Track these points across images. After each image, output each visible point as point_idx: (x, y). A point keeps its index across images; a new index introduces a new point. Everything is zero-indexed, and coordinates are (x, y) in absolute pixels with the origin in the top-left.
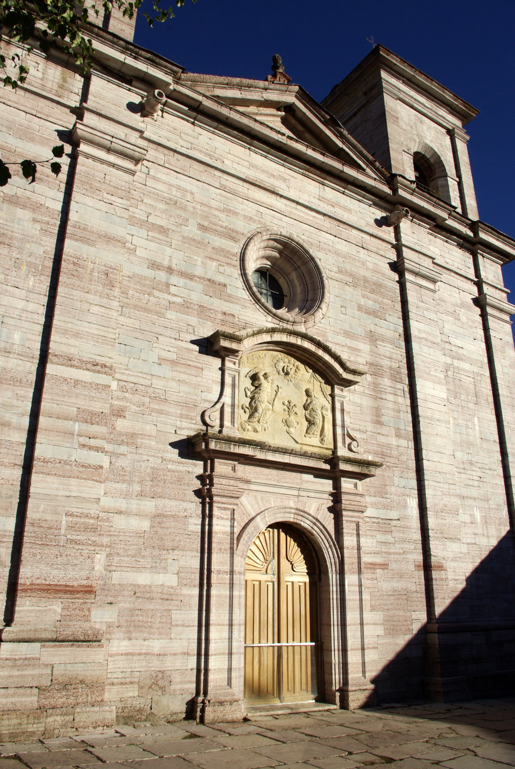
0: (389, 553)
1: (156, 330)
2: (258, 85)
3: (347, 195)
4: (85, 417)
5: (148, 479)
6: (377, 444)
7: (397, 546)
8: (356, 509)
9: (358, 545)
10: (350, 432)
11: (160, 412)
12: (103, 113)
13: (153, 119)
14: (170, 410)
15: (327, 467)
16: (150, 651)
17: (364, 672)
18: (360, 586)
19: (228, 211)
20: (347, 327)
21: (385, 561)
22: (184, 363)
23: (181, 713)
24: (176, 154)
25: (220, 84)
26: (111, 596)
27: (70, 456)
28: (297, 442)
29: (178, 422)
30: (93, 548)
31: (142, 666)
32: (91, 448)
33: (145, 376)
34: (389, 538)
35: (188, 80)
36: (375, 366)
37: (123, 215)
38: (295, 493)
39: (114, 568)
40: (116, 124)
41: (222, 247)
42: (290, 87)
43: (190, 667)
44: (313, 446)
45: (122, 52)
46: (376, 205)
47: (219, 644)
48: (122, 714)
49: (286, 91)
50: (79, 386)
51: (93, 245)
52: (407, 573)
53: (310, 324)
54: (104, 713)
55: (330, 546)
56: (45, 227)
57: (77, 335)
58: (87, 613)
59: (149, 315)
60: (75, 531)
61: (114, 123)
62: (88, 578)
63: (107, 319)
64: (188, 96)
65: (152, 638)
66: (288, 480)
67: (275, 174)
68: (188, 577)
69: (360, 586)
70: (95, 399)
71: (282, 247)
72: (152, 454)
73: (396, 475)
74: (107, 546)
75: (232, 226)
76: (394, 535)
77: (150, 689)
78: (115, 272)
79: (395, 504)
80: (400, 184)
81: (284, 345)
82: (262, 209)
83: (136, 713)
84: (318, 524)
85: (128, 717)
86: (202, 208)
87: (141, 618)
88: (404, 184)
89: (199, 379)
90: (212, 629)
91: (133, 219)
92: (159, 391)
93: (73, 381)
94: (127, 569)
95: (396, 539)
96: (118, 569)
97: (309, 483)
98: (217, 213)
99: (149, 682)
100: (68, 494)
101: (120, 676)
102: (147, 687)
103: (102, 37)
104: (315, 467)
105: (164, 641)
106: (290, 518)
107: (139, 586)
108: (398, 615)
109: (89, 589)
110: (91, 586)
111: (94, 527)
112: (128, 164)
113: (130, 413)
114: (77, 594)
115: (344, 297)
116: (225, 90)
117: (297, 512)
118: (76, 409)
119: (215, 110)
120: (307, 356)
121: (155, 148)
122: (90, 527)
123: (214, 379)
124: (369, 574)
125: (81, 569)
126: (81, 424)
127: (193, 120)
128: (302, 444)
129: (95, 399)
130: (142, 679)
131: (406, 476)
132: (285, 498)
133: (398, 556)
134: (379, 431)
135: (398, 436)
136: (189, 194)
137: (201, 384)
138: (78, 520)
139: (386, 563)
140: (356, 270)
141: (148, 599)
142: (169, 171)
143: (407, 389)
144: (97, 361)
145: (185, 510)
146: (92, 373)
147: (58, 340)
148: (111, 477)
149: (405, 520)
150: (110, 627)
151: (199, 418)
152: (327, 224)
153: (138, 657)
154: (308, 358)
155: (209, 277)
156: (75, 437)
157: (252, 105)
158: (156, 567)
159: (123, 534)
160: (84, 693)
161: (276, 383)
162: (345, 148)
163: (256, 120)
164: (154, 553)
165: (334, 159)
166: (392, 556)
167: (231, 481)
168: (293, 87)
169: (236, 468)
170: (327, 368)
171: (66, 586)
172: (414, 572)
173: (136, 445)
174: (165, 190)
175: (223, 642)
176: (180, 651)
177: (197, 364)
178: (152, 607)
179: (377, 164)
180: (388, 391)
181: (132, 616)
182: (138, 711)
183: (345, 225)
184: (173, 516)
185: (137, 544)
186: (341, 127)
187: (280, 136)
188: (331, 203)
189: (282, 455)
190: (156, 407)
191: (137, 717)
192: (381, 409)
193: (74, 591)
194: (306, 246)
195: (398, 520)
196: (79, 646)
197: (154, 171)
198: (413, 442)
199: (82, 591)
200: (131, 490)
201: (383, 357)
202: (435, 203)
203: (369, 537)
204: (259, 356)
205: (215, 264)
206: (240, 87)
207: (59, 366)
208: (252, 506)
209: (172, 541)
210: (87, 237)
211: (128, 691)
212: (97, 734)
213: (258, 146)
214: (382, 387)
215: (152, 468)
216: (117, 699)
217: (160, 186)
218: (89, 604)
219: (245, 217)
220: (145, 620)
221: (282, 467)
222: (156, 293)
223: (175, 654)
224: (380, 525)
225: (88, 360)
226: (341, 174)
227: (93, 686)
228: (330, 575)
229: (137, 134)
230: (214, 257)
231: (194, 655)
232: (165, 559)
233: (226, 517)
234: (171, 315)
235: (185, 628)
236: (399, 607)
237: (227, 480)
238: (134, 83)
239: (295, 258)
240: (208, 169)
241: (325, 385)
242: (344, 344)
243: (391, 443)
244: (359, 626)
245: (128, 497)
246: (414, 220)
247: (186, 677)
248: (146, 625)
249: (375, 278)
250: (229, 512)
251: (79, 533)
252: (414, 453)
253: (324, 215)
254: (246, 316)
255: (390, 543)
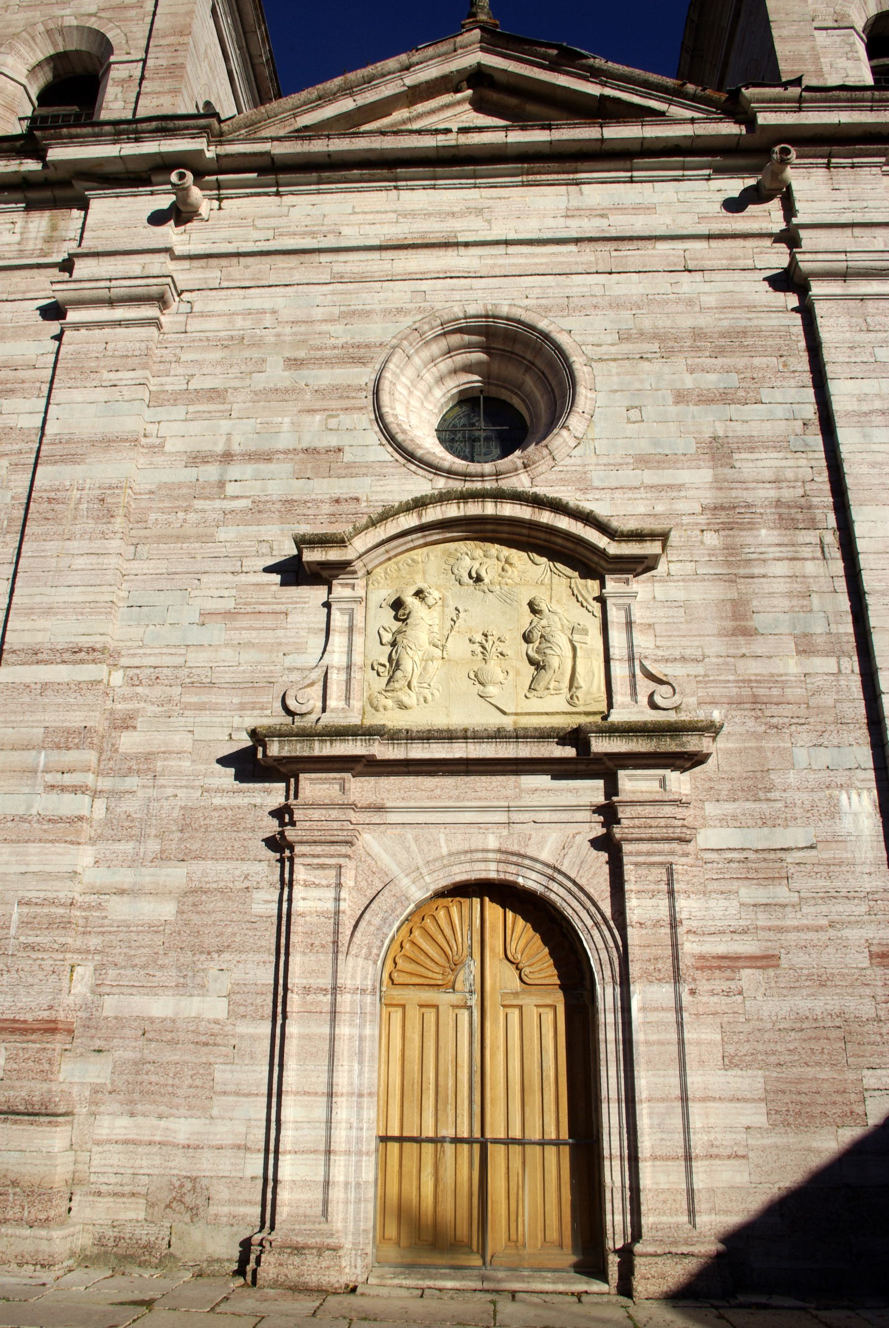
0: (781, 930)
1: (198, 567)
2: (386, 69)
3: (641, 182)
4: (56, 740)
5: (175, 828)
6: (737, 681)
7: (805, 909)
8: (658, 836)
9: (671, 915)
10: (649, 668)
11: (201, 707)
12: (100, 249)
13: (202, 220)
14: (220, 701)
15: (569, 752)
16: (170, 1139)
17: (692, 1212)
18: (679, 1009)
19: (349, 315)
20: (644, 447)
21: (767, 948)
22: (250, 610)
23: (228, 1260)
24: (242, 259)
25: (305, 104)
26: (100, 1038)
27: (29, 807)
28: (504, 713)
29: (237, 719)
30: (61, 956)
31: (154, 1166)
32: (63, 789)
33: (173, 651)
34: (781, 893)
35: (240, 128)
36: (730, 508)
37: (134, 396)
38: (502, 817)
39: (107, 989)
40: (126, 257)
41: (335, 383)
42: (459, 39)
43: (249, 1174)
44: (547, 714)
45: (115, 142)
46: (720, 171)
47: (306, 1132)
48: (115, 1249)
49: (455, 50)
50: (49, 692)
51: (82, 462)
52: (843, 975)
53: (542, 466)
54: (36, 1241)
55: (596, 924)
56: (15, 459)
57: (49, 611)
58: (46, 1067)
59: (185, 545)
60: (33, 929)
61: (122, 257)
62: (51, 1008)
63: (99, 572)
64: (245, 154)
65: (173, 1115)
66: (483, 794)
67: (455, 209)
68: (249, 1001)
69: (679, 1009)
70: (75, 707)
71: (483, 339)
72: (184, 783)
73: (801, 743)
74: (97, 952)
75: (358, 339)
76: (794, 885)
77: (168, 1210)
78: (117, 491)
79: (798, 811)
80: (758, 101)
81: (461, 525)
82: (425, 285)
83: (141, 1251)
84: (560, 878)
85: (126, 1257)
86: (294, 329)
87: (154, 1078)
88: (768, 96)
89: (280, 633)
90: (286, 1100)
91: (161, 396)
92: (199, 671)
93: (39, 686)
94: (130, 991)
95: (802, 895)
96: (115, 990)
97: (538, 793)
98: (325, 327)
99: (166, 1196)
100: (23, 869)
101: (113, 1179)
102: (163, 1206)
103: (77, 136)
104: (534, 756)
105: (198, 1121)
106: (491, 872)
107: (152, 1020)
108: (816, 1079)
109: (52, 1025)
110: (54, 1021)
111: (64, 920)
112: (149, 311)
113: (145, 719)
114: (32, 1034)
115: (637, 386)
116: (320, 110)
117: (503, 857)
118: (42, 730)
119: (298, 154)
120: (525, 531)
121: (204, 265)
122: (58, 920)
123: (312, 625)
124: (717, 982)
125: (40, 993)
126: (49, 752)
127: (274, 189)
128: (516, 714)
129: (75, 707)
130: (152, 1189)
131: (835, 742)
132: (477, 830)
133: (811, 935)
134: (743, 651)
135: (804, 651)
136: (268, 315)
137: (283, 640)
138: (39, 910)
139: (771, 952)
140: (669, 323)
141: (168, 1042)
142: (229, 292)
143: (831, 539)
144: (80, 645)
145: (246, 878)
146: (70, 667)
147: (19, 628)
148: (108, 832)
149: (834, 845)
150: (96, 1092)
151: (278, 705)
152: (587, 255)
153: (147, 1149)
154: (529, 536)
155: (305, 445)
156: (39, 774)
157: (395, 109)
158: (184, 985)
159: (125, 929)
160: (18, 1202)
161: (452, 603)
162: (608, 92)
163: (411, 132)
164: (182, 960)
165: (575, 126)
166: (792, 936)
167: (331, 812)
168: (466, 35)
169: (347, 786)
170: (577, 544)
171: (14, 1021)
172: (868, 972)
173: (155, 771)
174: (220, 326)
175: (315, 1128)
176: (230, 1142)
177: (275, 607)
178: (176, 1058)
179: (690, 88)
180: (771, 556)
181: (137, 1073)
182: (145, 1247)
183: (635, 242)
184: (221, 891)
185: (150, 946)
186: (586, 57)
187: (441, 137)
188: (599, 212)
189: (446, 745)
190: (194, 699)
191: (143, 1258)
192: (748, 602)
193: (26, 1030)
194: (525, 316)
195: (812, 847)
196: (15, 1122)
197: (200, 301)
198: (855, 658)
199: (39, 1029)
200: (142, 850)
201: (754, 485)
202: (872, 101)
203: (714, 895)
204: (413, 560)
205: (318, 417)
206: (348, 90)
207: (18, 667)
208: (393, 855)
209: (217, 936)
210: (73, 452)
211: (127, 1209)
212: (23, 1277)
213: (408, 175)
214: (752, 550)
215: (182, 808)
216: (105, 1222)
217: (211, 324)
218: (49, 1052)
219: (386, 312)
220: (162, 1081)
221: (463, 768)
222: (199, 504)
223: (220, 1148)
224: (750, 865)
225: (66, 646)
226: (606, 147)
227: (32, 1192)
228: (599, 988)
229: (164, 257)
230: (316, 407)
231: (259, 1150)
232: (203, 970)
233: (324, 882)
234: (226, 534)
235: (240, 1099)
236: (817, 1058)
237: (324, 811)
238: (154, 179)
239: (518, 349)
240: (306, 258)
241: (583, 581)
242: (638, 484)
243: (782, 672)
244: (679, 1104)
245: (136, 864)
246: (833, 160)
247: (240, 1192)
248: (163, 1091)
249: (725, 323)
250: (333, 872)
251: (39, 932)
252: (859, 684)
253: (577, 241)
254: (384, 492)
255: (784, 906)
